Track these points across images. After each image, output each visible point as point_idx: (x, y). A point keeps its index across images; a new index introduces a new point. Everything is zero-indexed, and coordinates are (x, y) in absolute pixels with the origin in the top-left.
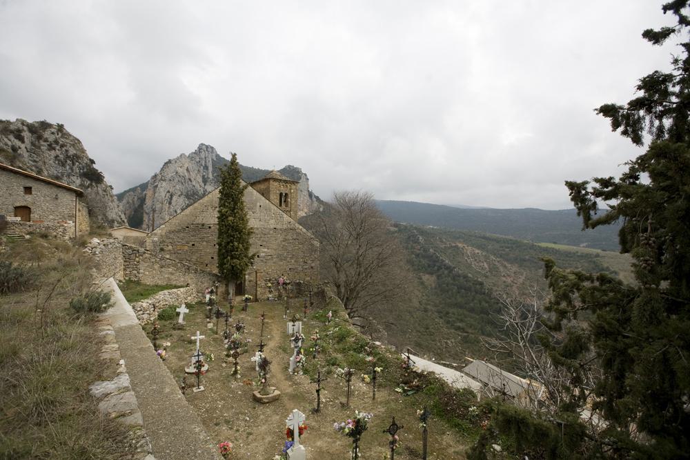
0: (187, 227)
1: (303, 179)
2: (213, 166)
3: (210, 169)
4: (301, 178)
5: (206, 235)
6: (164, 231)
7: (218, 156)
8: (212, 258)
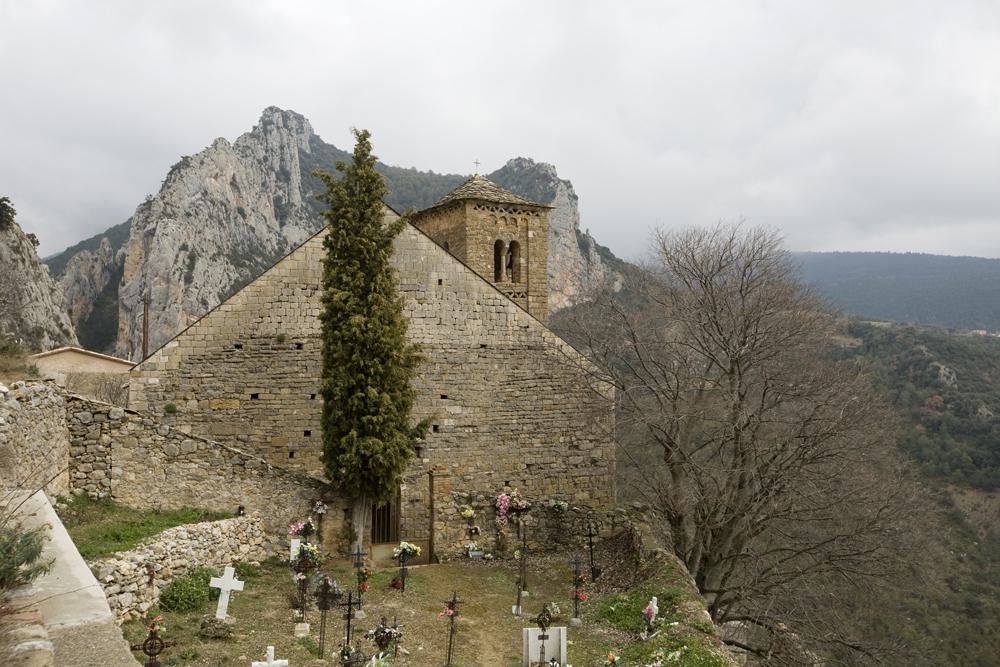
0: (238, 347)
1: (561, 198)
2: (305, 170)
3: (296, 178)
7: (315, 140)
8: (307, 433)
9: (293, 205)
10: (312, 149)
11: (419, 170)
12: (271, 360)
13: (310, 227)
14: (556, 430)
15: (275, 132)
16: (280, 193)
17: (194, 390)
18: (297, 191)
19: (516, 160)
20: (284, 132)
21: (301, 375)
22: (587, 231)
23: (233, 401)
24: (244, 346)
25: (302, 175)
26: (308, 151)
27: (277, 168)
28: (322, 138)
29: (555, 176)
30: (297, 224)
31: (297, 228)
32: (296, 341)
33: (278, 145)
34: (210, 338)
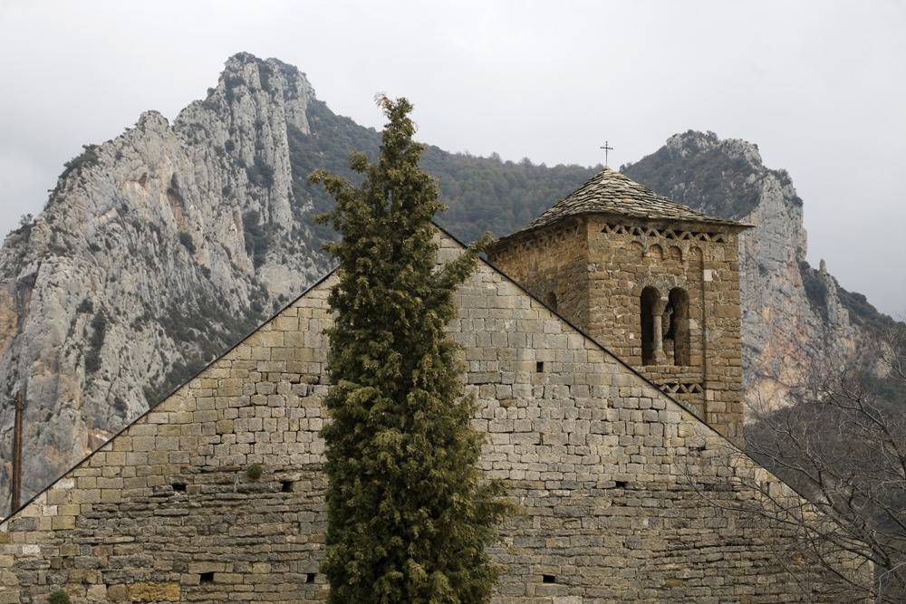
0: (179, 487)
1: (770, 203)
2: (298, 165)
3: (284, 179)
4: (755, 199)
5: (264, 527)
6: (72, 510)
7: (317, 110)
9: (279, 226)
10: (312, 126)
12: (236, 511)
13: (307, 266)
15: (247, 98)
16: (256, 206)
17: (100, 568)
18: (286, 202)
19: (684, 136)
20: (263, 97)
21: (289, 538)
22: (822, 263)
25: (295, 173)
26: (305, 131)
27: (250, 161)
28: (330, 106)
29: (757, 162)
30: (284, 261)
31: (285, 267)
32: (280, 476)
33: (252, 120)
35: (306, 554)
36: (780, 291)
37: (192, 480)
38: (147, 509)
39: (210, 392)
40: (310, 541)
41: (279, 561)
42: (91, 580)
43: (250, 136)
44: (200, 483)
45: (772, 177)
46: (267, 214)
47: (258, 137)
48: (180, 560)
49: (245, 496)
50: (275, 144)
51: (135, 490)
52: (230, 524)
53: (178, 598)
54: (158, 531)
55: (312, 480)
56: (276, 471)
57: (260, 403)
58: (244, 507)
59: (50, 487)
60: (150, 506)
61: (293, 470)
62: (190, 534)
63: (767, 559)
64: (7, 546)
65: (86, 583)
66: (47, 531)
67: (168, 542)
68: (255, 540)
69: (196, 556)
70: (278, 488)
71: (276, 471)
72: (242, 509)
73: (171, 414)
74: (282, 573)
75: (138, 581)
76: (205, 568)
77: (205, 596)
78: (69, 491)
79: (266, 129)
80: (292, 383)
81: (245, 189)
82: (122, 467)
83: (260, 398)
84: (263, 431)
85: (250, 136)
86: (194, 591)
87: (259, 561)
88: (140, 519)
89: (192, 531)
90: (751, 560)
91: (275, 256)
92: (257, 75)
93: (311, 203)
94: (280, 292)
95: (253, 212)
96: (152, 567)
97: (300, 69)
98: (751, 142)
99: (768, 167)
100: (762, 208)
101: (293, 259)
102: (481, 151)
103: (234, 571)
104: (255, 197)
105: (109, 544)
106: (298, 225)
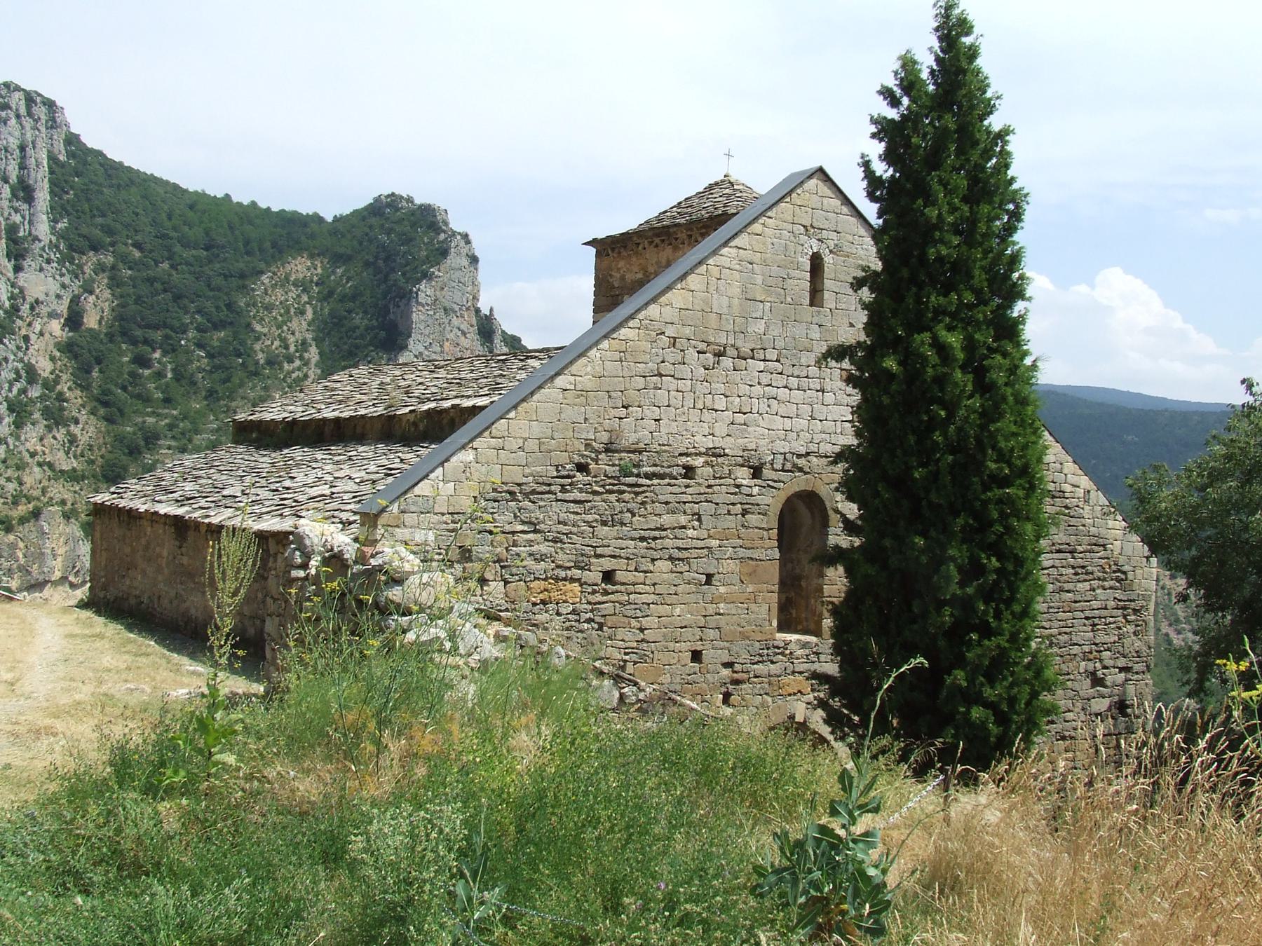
0: (582, 468)
1: (455, 260)
2: (57, 187)
3: (43, 196)
4: (444, 253)
5: (667, 520)
6: (470, 489)
7: (72, 140)
8: (696, 656)
9: (36, 239)
10: (71, 155)
11: (235, 199)
12: (640, 498)
13: (62, 275)
14: (1076, 650)
15: (13, 121)
16: (17, 218)
17: (499, 561)
18: (44, 217)
19: (388, 196)
20: (28, 123)
21: (690, 532)
22: (491, 310)
23: (569, 586)
24: (592, 466)
25: (52, 192)
26: (62, 158)
27: (13, 178)
28: (84, 139)
29: (446, 224)
30: (41, 270)
31: (42, 275)
32: (684, 460)
33: (17, 142)
34: (532, 445)
35: (705, 552)
36: (459, 329)
37: (596, 461)
38: (549, 492)
39: (617, 356)
40: (710, 537)
41: (679, 559)
42: (488, 576)
43: (14, 156)
44: (604, 466)
45: (459, 237)
46: (27, 227)
47: (21, 158)
48: (582, 555)
49: (648, 482)
50: (37, 166)
51: (539, 469)
52: (633, 515)
53: (578, 600)
54: (561, 520)
55: (713, 466)
56: (681, 455)
57: (668, 373)
58: (647, 494)
59: (447, 460)
60: (553, 488)
61: (696, 454)
62: (594, 524)
63: (1083, 567)
64: (397, 530)
65: (483, 581)
66: (443, 514)
67: (571, 533)
68: (657, 533)
69: (599, 551)
70: (681, 475)
71: (681, 455)
72: (646, 497)
73: (577, 378)
74: (682, 573)
75: (538, 579)
76: (608, 564)
77: (605, 599)
78: (467, 466)
79: (29, 151)
80: (698, 352)
81: (8, 203)
82: (525, 439)
83: (666, 368)
84: (668, 406)
85: (14, 156)
86: (594, 592)
87: (660, 559)
88: (542, 503)
89: (596, 521)
90: (1073, 567)
91: (33, 264)
92: (23, 102)
93: (65, 221)
94: (36, 296)
95: (15, 223)
96: (553, 562)
97: (59, 104)
98: (443, 207)
99: (454, 229)
100: (449, 261)
101: (50, 269)
102: (216, 191)
103: (636, 570)
104: (17, 211)
105: (508, 533)
106: (54, 239)
